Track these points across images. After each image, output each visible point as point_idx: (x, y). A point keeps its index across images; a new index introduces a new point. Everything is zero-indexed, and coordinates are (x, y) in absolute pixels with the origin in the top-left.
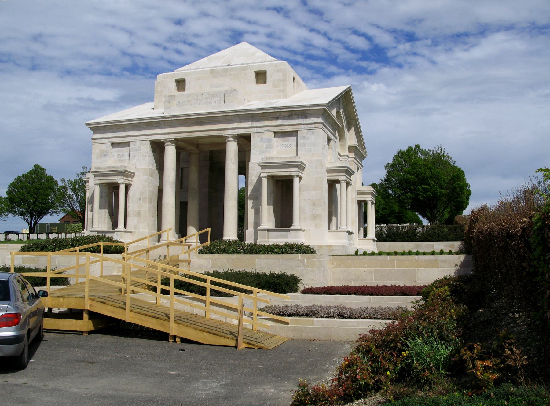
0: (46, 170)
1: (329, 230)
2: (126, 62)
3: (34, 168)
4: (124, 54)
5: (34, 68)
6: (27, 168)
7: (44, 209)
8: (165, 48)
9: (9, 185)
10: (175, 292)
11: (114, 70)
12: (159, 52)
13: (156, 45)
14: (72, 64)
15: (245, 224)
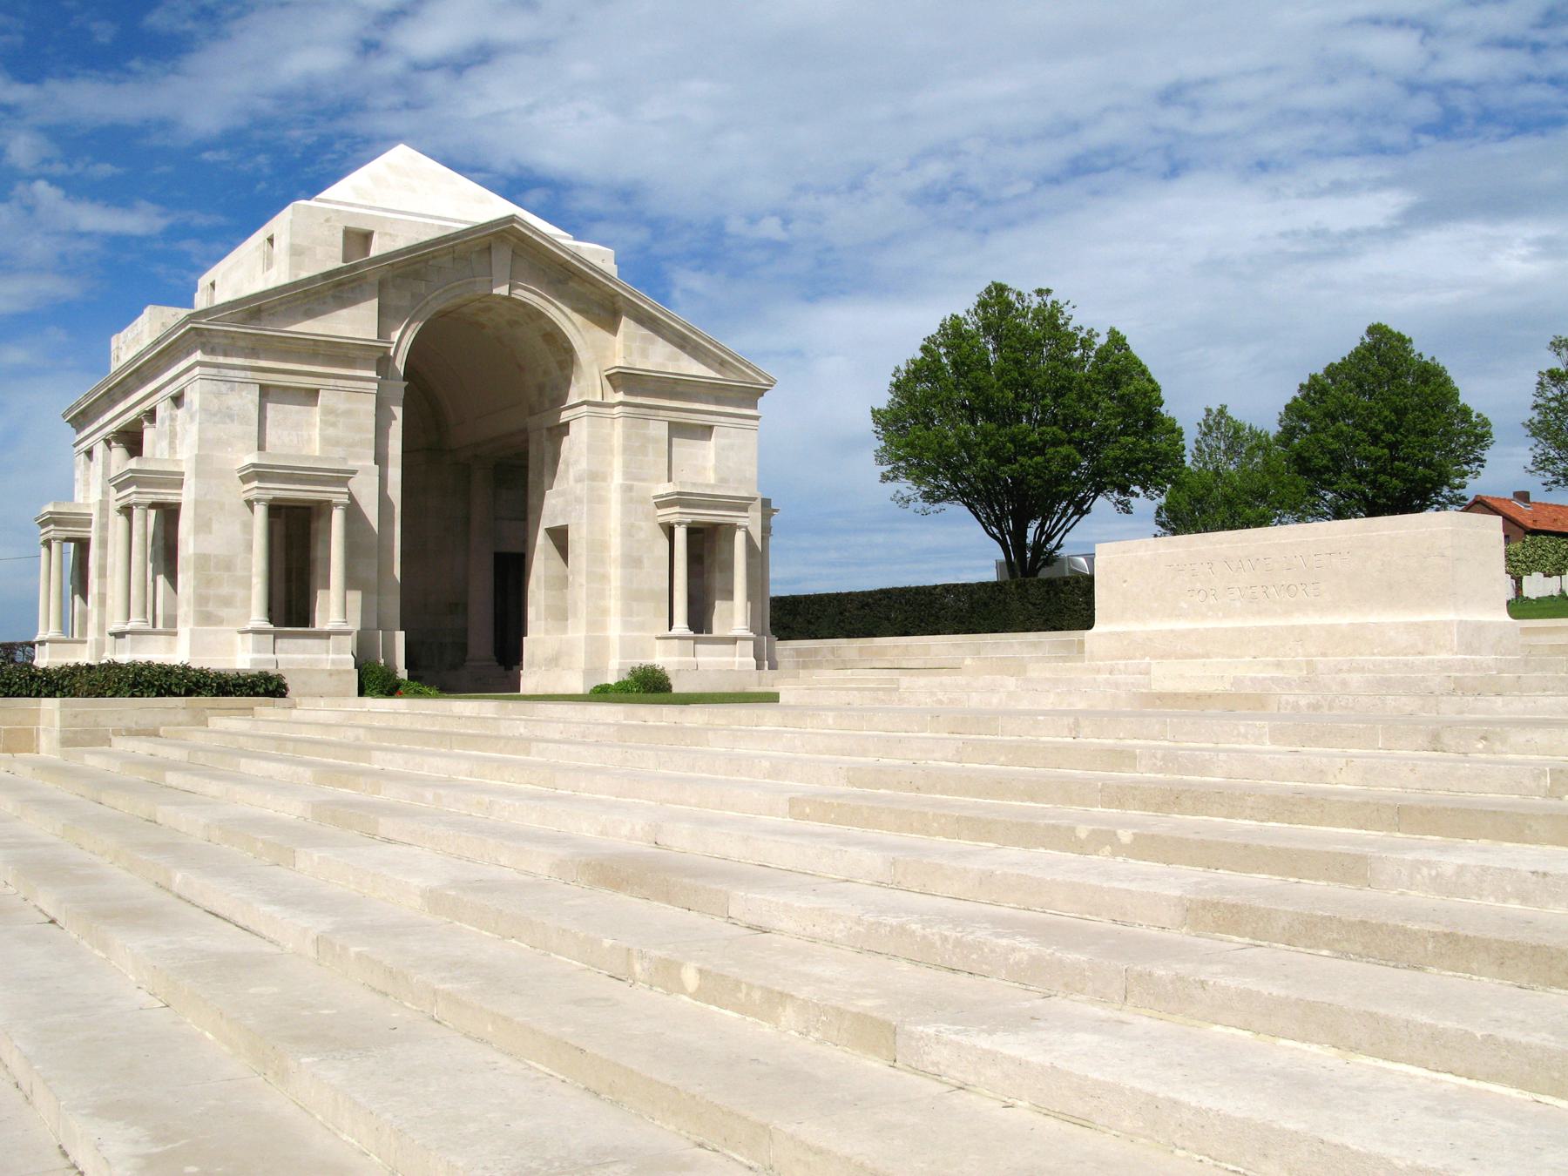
0: (1410, 341)
1: (167, 496)
2: (1424, 108)
3: (1367, 340)
4: (1413, 88)
5: (1175, 170)
6: (1343, 343)
7: (1429, 486)
8: (1536, 48)
9: (1283, 410)
10: (214, 281)
11: (1392, 136)
12: (1519, 61)
13: (1507, 44)
14: (1270, 143)
15: (283, 504)
